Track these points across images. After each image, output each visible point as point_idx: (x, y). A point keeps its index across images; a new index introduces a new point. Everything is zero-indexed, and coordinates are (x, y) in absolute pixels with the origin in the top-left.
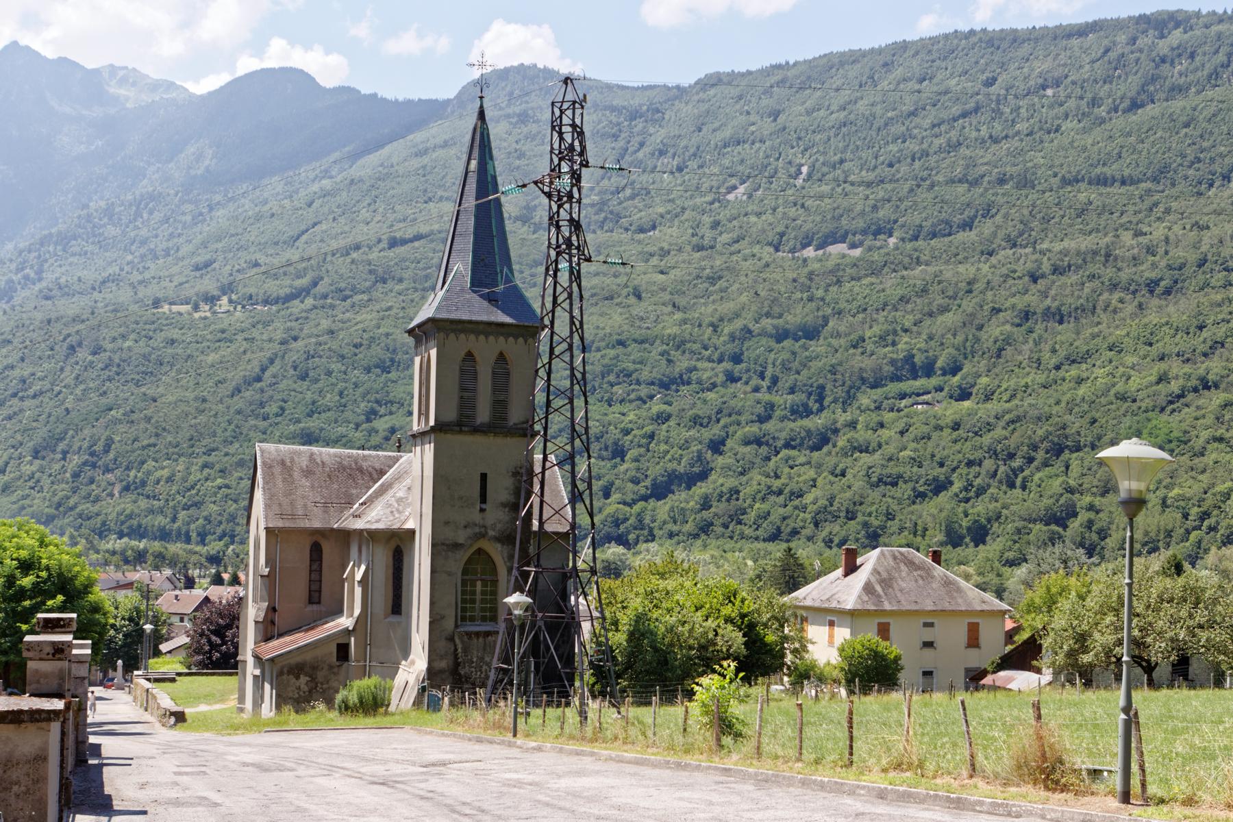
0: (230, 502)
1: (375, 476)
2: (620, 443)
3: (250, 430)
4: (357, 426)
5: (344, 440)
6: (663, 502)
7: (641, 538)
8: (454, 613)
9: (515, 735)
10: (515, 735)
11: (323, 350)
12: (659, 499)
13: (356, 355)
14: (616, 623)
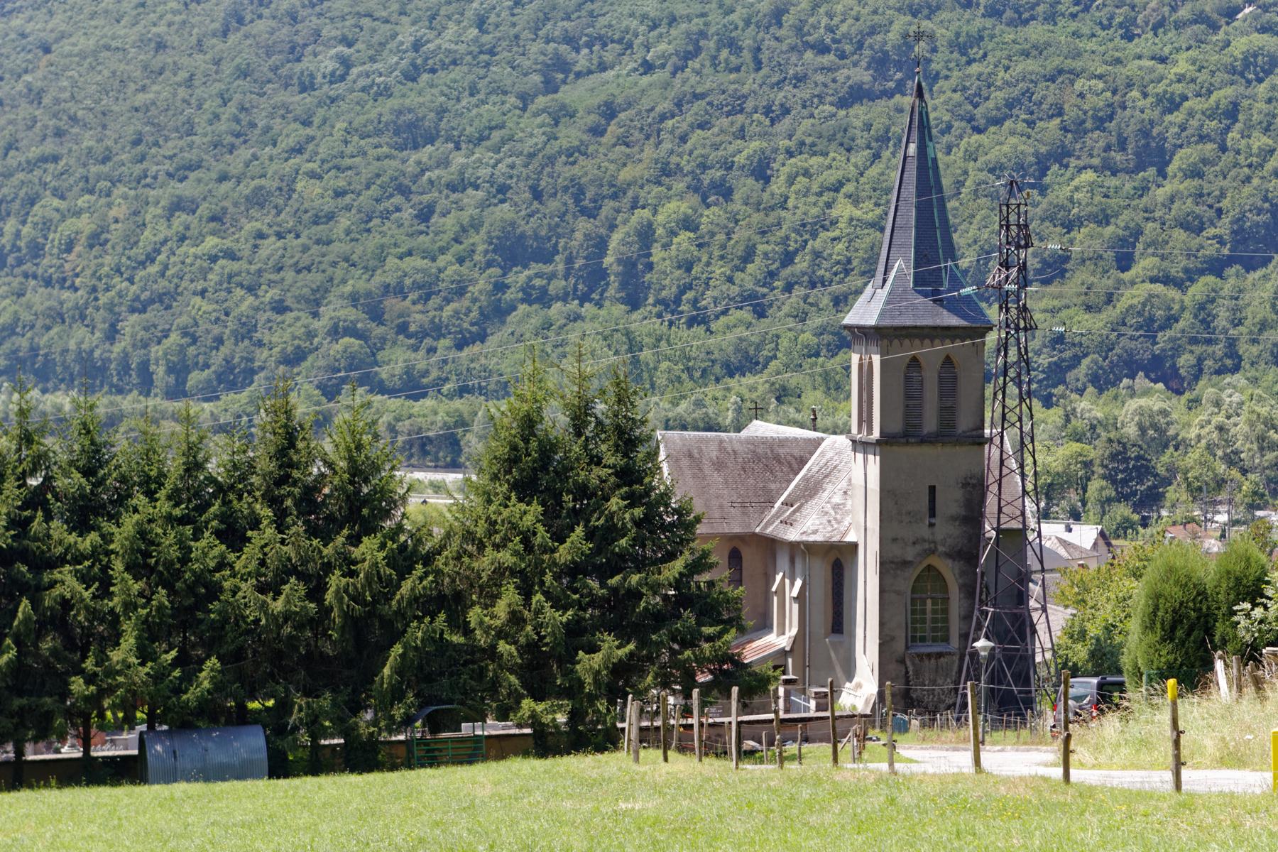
0: (239, 292)
1: (795, 466)
2: (1155, 132)
3: (271, 116)
4: (525, 99)
5: (496, 136)
6: (1259, 273)
7: (1209, 363)
12: (1250, 266)
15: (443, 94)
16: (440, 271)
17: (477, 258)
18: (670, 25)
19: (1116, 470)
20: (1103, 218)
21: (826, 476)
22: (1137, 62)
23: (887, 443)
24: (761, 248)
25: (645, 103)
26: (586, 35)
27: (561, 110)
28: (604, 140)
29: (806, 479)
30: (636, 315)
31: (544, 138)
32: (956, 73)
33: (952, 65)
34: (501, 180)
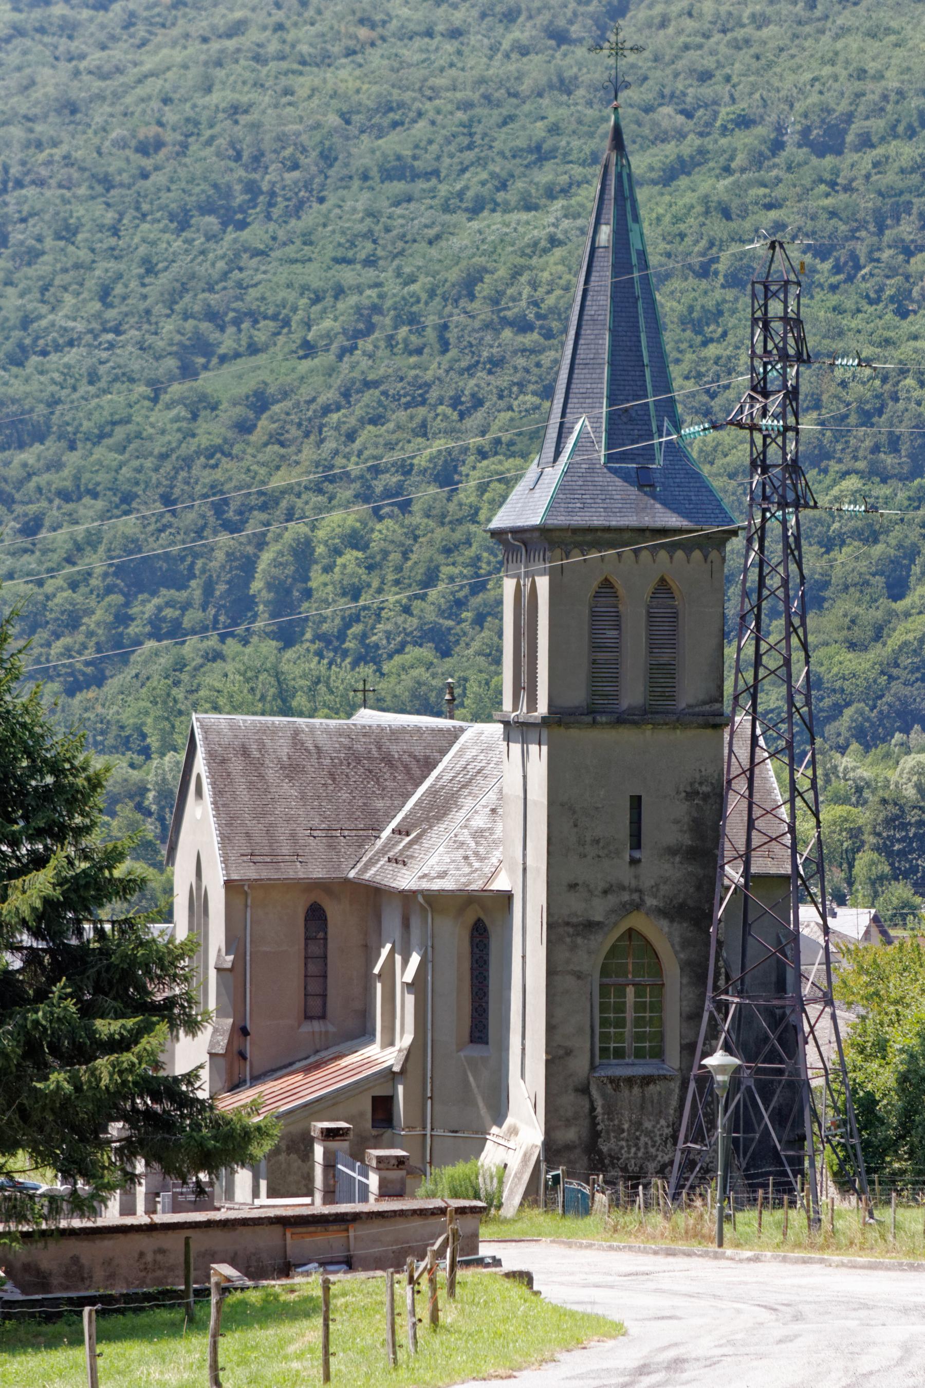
1: (416, 771)
4: (157, 389)
5: (120, 433)
8: (588, 1045)
9: (721, 1245)
10: (721, 1245)
11: (49, 163)
13: (145, 176)
14: (882, 1046)
15: (53, 381)
16: (48, 598)
17: (94, 582)
18: (336, 297)
19: (891, 838)
20: (871, 536)
21: (464, 787)
22: (912, 343)
23: (559, 723)
24: (446, 570)
25: (305, 392)
26: (234, 310)
27: (200, 401)
28: (253, 438)
29: (433, 792)
30: (290, 654)
31: (179, 436)
32: (689, 356)
33: (684, 346)
34: (126, 487)
